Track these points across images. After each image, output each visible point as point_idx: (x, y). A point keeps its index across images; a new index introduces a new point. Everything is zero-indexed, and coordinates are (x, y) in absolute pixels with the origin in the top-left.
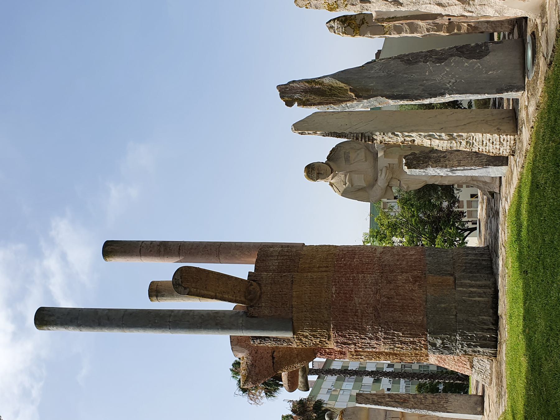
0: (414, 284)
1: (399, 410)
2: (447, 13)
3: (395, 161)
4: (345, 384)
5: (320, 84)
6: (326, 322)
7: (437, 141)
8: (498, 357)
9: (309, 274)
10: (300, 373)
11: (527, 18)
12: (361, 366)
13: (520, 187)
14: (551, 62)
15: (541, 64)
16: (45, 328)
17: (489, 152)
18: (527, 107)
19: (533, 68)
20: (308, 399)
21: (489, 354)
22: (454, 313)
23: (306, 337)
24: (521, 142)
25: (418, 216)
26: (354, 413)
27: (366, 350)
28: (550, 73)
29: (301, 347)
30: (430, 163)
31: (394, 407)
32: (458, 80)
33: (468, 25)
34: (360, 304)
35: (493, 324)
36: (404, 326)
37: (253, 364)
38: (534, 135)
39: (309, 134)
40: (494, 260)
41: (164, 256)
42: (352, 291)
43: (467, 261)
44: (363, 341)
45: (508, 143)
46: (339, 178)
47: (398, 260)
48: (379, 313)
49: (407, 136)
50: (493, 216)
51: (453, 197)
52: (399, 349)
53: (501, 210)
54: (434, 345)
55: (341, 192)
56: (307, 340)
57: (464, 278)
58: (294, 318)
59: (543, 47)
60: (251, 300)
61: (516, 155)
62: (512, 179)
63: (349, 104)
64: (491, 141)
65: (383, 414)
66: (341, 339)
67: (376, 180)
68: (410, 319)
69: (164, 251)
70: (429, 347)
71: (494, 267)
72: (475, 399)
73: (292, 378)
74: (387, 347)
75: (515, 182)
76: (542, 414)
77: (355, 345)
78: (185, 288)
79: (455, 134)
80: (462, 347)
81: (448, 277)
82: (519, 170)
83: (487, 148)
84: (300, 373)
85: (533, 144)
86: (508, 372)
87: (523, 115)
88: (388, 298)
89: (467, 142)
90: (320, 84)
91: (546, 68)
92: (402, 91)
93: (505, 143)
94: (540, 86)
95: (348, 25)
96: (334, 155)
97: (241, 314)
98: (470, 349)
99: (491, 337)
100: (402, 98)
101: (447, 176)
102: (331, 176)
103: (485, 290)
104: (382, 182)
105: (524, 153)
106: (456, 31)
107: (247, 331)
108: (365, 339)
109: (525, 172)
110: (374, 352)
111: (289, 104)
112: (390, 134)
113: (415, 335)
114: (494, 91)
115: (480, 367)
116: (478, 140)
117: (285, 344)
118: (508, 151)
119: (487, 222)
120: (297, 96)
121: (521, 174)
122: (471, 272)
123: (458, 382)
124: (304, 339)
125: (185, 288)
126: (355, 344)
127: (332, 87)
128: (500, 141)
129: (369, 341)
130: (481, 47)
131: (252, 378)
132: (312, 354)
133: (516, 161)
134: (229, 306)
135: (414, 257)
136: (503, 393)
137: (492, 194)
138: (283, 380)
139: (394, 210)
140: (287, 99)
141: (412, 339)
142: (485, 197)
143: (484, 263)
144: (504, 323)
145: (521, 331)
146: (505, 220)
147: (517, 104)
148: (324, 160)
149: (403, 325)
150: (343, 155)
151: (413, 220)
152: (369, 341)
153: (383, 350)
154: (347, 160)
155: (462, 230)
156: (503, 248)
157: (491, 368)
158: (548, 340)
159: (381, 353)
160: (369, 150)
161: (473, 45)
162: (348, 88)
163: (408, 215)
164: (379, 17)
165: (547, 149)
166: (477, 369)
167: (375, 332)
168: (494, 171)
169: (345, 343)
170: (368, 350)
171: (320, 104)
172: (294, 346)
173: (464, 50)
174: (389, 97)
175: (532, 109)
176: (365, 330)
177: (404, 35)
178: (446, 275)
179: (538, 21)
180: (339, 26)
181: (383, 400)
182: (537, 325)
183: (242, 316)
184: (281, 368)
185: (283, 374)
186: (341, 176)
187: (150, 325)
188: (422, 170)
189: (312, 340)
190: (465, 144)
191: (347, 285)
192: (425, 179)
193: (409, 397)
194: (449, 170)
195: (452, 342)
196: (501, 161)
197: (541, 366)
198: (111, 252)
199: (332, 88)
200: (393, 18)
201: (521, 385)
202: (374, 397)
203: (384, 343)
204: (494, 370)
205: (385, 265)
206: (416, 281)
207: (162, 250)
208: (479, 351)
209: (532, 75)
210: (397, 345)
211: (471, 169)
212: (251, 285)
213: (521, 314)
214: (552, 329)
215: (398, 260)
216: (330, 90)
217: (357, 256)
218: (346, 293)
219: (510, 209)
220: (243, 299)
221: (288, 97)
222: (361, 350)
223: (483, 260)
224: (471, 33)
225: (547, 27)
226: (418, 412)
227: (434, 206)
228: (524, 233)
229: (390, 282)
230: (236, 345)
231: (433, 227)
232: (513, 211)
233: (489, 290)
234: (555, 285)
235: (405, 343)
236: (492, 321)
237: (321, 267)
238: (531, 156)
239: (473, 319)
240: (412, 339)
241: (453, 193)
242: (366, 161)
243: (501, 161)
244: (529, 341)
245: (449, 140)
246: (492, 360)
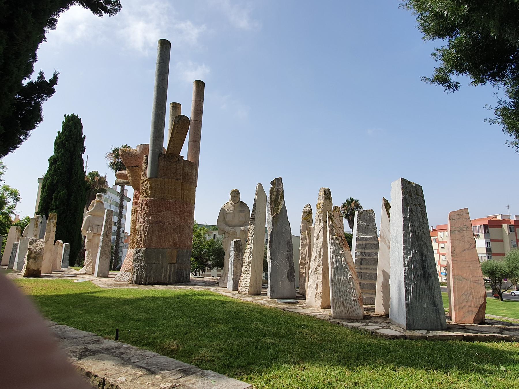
0: (173, 243)
1: (102, 233)
2: (311, 261)
3: (238, 236)
4: (114, 206)
5: (281, 199)
6: (154, 196)
7: (248, 256)
8: (131, 285)
9: (181, 189)
10: (126, 180)
11: (306, 300)
12: (124, 216)
13: (222, 296)
14: (285, 310)
15: (284, 306)
16: (159, 44)
17: (241, 281)
18: (263, 299)
19: (282, 302)
20: (107, 186)
21: (132, 280)
22: (156, 263)
23: (146, 185)
24: (245, 297)
25: (204, 249)
26: (101, 208)
27: (138, 216)
28: (280, 310)
29: (141, 181)
30: (236, 253)
31: (104, 230)
32: (278, 266)
33: (303, 272)
34: (163, 214)
35: (149, 282)
36: (150, 237)
37: (132, 155)
38: (249, 303)
39: (256, 192)
40: (183, 284)
41: (195, 112)
42: (171, 210)
43: (183, 270)
44: (143, 215)
45: (245, 291)
46: (231, 207)
47: (185, 235)
48: (158, 223)
49: (251, 241)
50: (206, 284)
51: (213, 267)
52: (137, 233)
53: (210, 287)
54: (139, 251)
55: (224, 208)
56: (145, 185)
57: (174, 268)
58: (157, 179)
59: (292, 307)
60: (168, 157)
61: (238, 294)
62: (226, 292)
63: (270, 213)
64: (246, 282)
65: (100, 224)
66: (144, 203)
67: (229, 226)
68: (154, 240)
69: (197, 113)
70: (138, 249)
71: (179, 284)
72: (106, 273)
73: (124, 176)
74: (139, 227)
75: (225, 294)
76: (101, 305)
77: (140, 210)
78: (178, 121)
79: (251, 265)
80: (137, 266)
81: (175, 260)
82: (231, 296)
83: (243, 280)
84: (125, 181)
85: (244, 302)
86: (123, 289)
87: (258, 297)
88: (166, 229)
89: (246, 271)
90: (281, 199)
91: (282, 308)
92: (274, 239)
93: (245, 289)
94: (273, 306)
95: (307, 215)
96: (243, 205)
97: (161, 151)
98: (136, 270)
99: (142, 281)
100: (271, 239)
101: (229, 261)
102: (232, 203)
103: (167, 279)
104: (227, 228)
105: (240, 298)
106: (301, 266)
107: (151, 154)
108: (144, 216)
109: (230, 298)
110: (136, 220)
111: (272, 183)
112: (253, 233)
113: (145, 242)
114: (271, 284)
115: (125, 275)
116: (247, 276)
117: (143, 173)
118: (241, 291)
119: (203, 281)
120: (276, 187)
121: (229, 297)
122: (177, 272)
123: (113, 267)
124: (145, 183)
125: (178, 121)
126: (141, 210)
127: (279, 205)
128: (246, 287)
129: (142, 218)
130: (293, 278)
131: (124, 154)
132: (137, 187)
133: (235, 294)
134: (166, 145)
135: (187, 243)
136: (110, 287)
137: (218, 283)
138: (119, 171)
139: (208, 237)
140: (275, 181)
141: (143, 240)
142: (216, 280)
143: (182, 279)
144: (149, 288)
145: (147, 295)
146: (205, 289)
147: (264, 295)
148: (241, 200)
149: (151, 236)
150: (243, 210)
151: (202, 246)
152: (142, 218)
153: (137, 225)
154: (241, 212)
155: (196, 271)
156: (190, 288)
157: (124, 281)
158: (142, 308)
159: (135, 224)
160: (245, 223)
161: (294, 274)
162: (278, 213)
163: (205, 243)
164: (311, 229)
165: (242, 308)
166: (124, 274)
167: (148, 221)
168: (230, 284)
169: (142, 205)
170: (138, 217)
171: (271, 198)
172: (142, 178)
173: (292, 270)
174: (272, 232)
175: (262, 302)
176: (149, 216)
177: (301, 241)
178: (177, 259)
179: (304, 305)
180: (307, 210)
181: (108, 224)
182: (151, 303)
183: (160, 151)
184: (129, 170)
185: (126, 171)
186: (232, 208)
187: (158, 101)
188: (233, 248)
189: (144, 187)
190: (246, 270)
191: (174, 208)
192: (228, 250)
193: (109, 238)
194: (232, 261)
195: (140, 261)
196: (236, 287)
197: (128, 304)
198: (198, 85)
199: (278, 204)
200: (310, 236)
201: (117, 295)
202: (110, 220)
203: (141, 226)
204: (123, 283)
205: (183, 229)
206: (174, 244)
207: (198, 112)
208: (134, 275)
209: (279, 301)
210: (140, 232)
211: (232, 273)
212: (177, 157)
213: (155, 296)
214: (149, 310)
215: (185, 235)
216: (278, 204)
217: (189, 214)
218: (169, 207)
219: (210, 291)
220: (169, 152)
221: (276, 182)
222: (138, 213)
223: (183, 278)
224: (299, 274)
225: (301, 308)
226: (101, 242)
227: (209, 257)
228: (199, 297)
229: (174, 230)
230: (144, 147)
231: (198, 256)
232: (210, 293)
233: (167, 281)
234: (172, 311)
235: (141, 237)
236: (151, 282)
237: (184, 195)
238: (238, 301)
239: (152, 272)
240: (143, 240)
241: (216, 267)
242: (239, 221)
243: (236, 287)
244: (142, 299)
245: (248, 262)
246: (129, 282)
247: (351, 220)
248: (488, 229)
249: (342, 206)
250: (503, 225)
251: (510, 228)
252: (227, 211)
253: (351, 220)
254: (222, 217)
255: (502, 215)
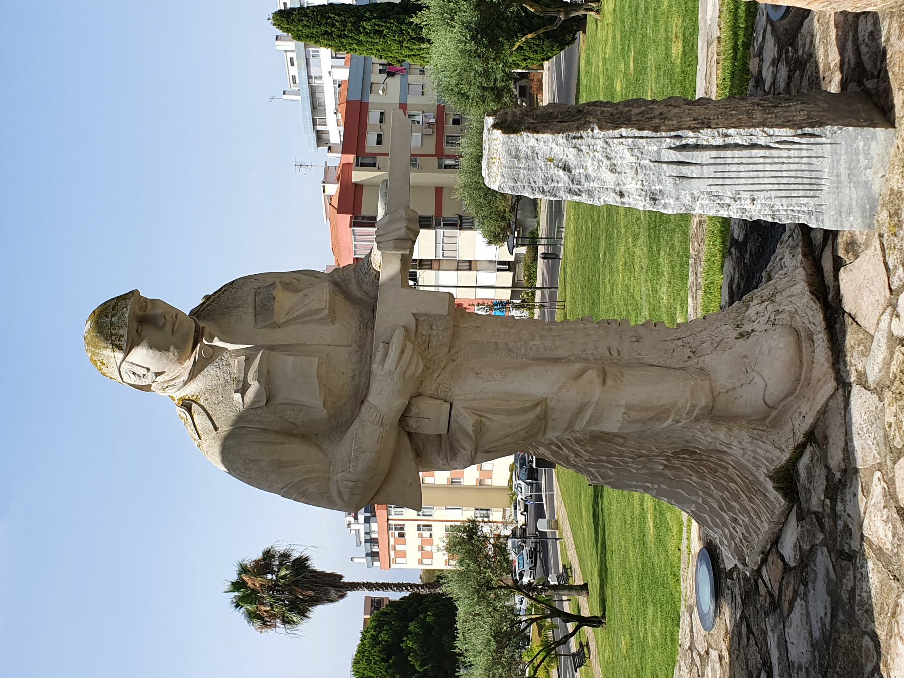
150: (250, 299)
247: (312, 593)
248: (364, 218)
249: (258, 623)
250: (353, 181)
251: (362, 165)
252: (250, 394)
253: (312, 593)
254: (296, 450)
255: (324, 182)
